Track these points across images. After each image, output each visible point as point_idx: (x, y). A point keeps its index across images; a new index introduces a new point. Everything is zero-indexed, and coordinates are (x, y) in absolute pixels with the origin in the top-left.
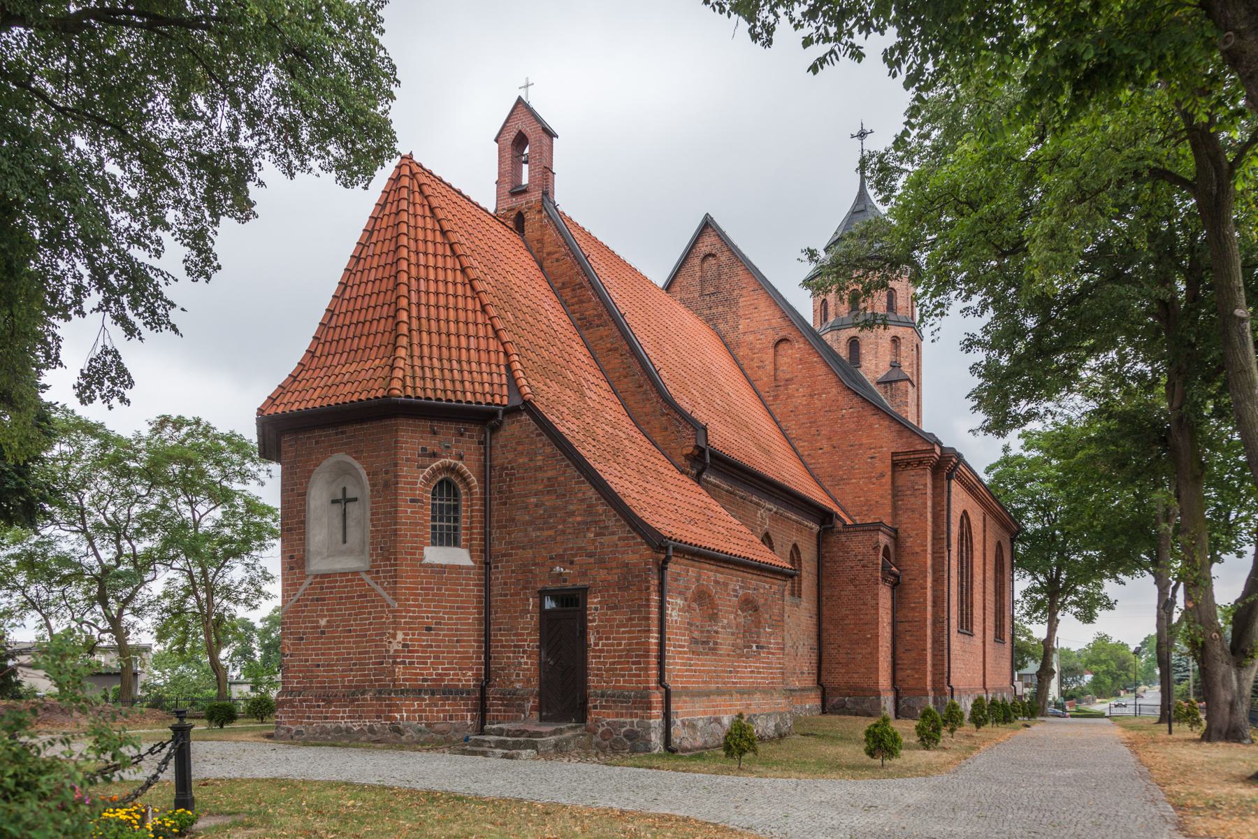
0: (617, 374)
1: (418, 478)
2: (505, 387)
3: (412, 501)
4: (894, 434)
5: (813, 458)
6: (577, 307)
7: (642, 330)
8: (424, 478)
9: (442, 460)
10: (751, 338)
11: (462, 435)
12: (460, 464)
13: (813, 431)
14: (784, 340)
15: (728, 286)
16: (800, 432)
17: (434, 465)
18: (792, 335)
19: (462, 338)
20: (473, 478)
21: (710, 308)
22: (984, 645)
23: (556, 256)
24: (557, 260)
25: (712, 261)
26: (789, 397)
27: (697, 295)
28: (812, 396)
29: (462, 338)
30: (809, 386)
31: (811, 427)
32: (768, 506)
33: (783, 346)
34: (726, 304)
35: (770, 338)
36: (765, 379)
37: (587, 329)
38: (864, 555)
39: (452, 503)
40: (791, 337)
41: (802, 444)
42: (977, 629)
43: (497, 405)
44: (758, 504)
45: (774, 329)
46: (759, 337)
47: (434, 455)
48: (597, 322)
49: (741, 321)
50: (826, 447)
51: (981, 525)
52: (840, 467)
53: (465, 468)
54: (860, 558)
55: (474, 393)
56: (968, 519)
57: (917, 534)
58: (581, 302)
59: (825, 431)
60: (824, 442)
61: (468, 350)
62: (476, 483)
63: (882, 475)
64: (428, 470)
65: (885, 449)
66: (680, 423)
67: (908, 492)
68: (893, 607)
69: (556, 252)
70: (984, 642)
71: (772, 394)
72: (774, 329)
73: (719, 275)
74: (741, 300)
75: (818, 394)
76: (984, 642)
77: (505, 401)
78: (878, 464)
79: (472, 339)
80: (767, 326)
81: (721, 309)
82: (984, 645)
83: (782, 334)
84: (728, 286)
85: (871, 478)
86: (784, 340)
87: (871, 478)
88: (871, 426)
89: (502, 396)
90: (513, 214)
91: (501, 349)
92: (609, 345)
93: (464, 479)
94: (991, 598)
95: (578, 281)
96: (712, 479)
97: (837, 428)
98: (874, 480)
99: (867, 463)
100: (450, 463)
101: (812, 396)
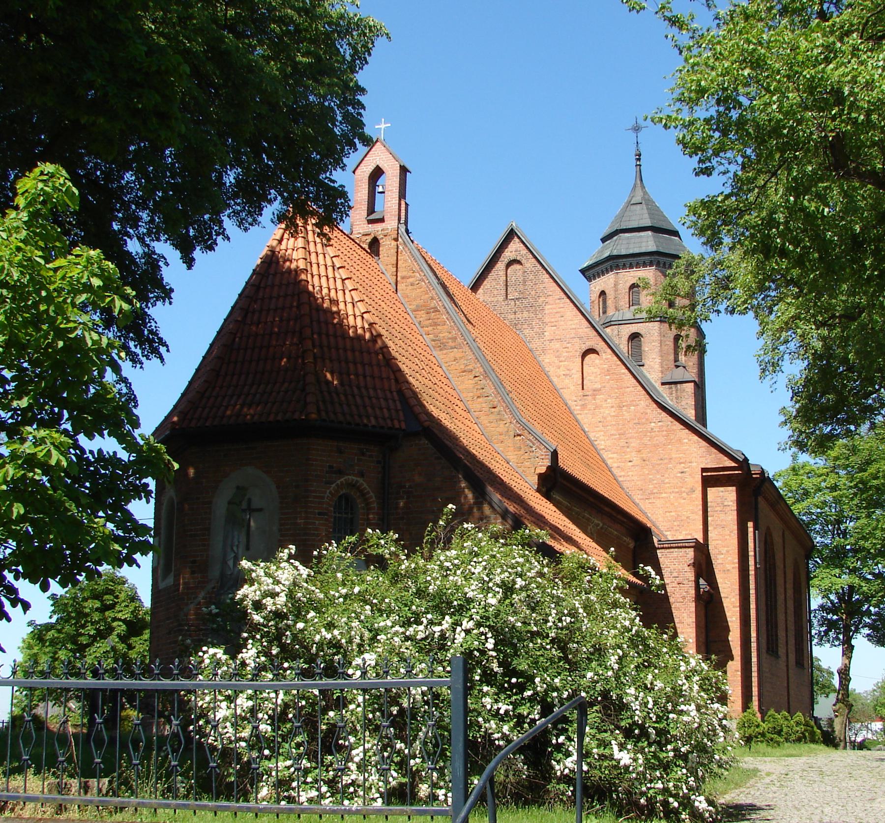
0: (471, 394)
1: (325, 493)
2: (401, 413)
3: (320, 514)
4: (703, 449)
5: (623, 470)
6: (431, 328)
7: (376, 293)
8: (330, 493)
9: (346, 477)
10: (557, 345)
11: (363, 454)
12: (361, 480)
13: (622, 443)
14: (591, 351)
15: (533, 293)
16: (609, 443)
17: (339, 482)
18: (600, 345)
19: (359, 366)
20: (372, 494)
21: (515, 313)
22: (788, 670)
23: (411, 280)
24: (412, 285)
25: (516, 267)
26: (597, 407)
27: (501, 298)
28: (620, 407)
29: (359, 366)
30: (617, 397)
31: (620, 439)
32: (596, 521)
33: (592, 356)
34: (532, 310)
35: (577, 348)
36: (572, 388)
37: (441, 350)
38: (679, 572)
39: (350, 516)
40: (597, 348)
41: (612, 456)
42: (782, 651)
43: (397, 429)
44: (588, 519)
45: (581, 338)
46: (565, 345)
47: (340, 473)
48: (451, 344)
49: (547, 328)
50: (636, 461)
51: (781, 541)
52: (651, 481)
53: (365, 485)
54: (675, 574)
55: (376, 418)
56: (771, 535)
57: (728, 551)
58: (436, 324)
59: (634, 443)
60: (634, 454)
61: (365, 377)
62: (374, 499)
63: (693, 491)
64: (334, 485)
65: (694, 464)
66: (534, 444)
67: (718, 509)
68: (706, 626)
69: (410, 277)
70: (787, 666)
71: (580, 403)
72: (581, 338)
73: (525, 281)
74: (547, 307)
75: (626, 406)
76: (787, 666)
77: (404, 426)
78: (689, 480)
79: (367, 366)
80: (573, 335)
81: (526, 314)
82: (788, 670)
83: (588, 345)
84: (533, 293)
85: (681, 493)
86: (591, 351)
87: (681, 493)
88: (680, 441)
89: (399, 422)
90: (369, 239)
91: (392, 377)
92: (462, 367)
93: (363, 494)
94: (791, 619)
95: (432, 305)
96: (558, 498)
97: (646, 440)
98: (684, 495)
99: (677, 477)
100: (353, 480)
101: (620, 407)
